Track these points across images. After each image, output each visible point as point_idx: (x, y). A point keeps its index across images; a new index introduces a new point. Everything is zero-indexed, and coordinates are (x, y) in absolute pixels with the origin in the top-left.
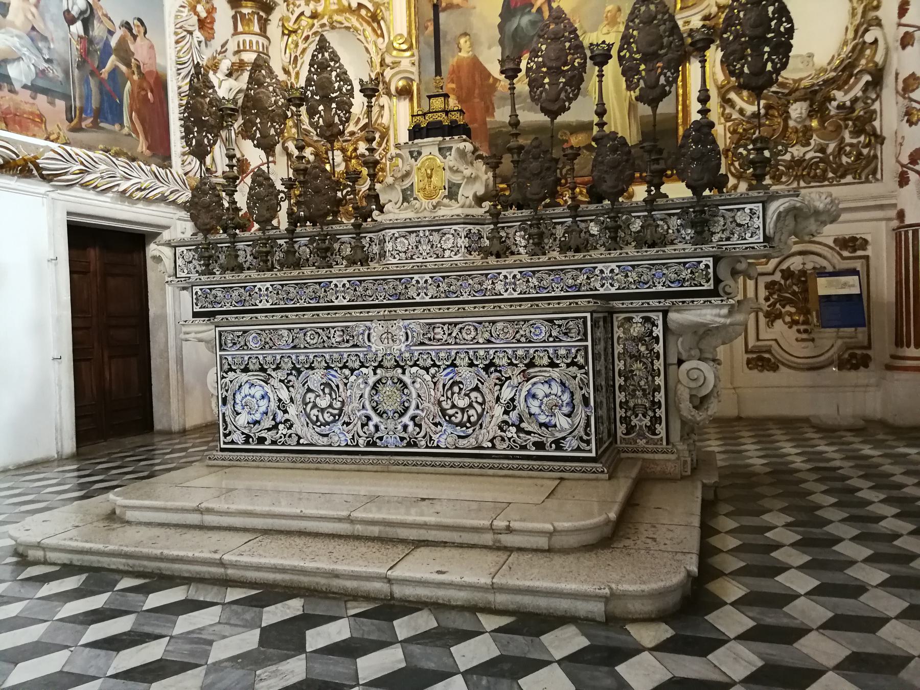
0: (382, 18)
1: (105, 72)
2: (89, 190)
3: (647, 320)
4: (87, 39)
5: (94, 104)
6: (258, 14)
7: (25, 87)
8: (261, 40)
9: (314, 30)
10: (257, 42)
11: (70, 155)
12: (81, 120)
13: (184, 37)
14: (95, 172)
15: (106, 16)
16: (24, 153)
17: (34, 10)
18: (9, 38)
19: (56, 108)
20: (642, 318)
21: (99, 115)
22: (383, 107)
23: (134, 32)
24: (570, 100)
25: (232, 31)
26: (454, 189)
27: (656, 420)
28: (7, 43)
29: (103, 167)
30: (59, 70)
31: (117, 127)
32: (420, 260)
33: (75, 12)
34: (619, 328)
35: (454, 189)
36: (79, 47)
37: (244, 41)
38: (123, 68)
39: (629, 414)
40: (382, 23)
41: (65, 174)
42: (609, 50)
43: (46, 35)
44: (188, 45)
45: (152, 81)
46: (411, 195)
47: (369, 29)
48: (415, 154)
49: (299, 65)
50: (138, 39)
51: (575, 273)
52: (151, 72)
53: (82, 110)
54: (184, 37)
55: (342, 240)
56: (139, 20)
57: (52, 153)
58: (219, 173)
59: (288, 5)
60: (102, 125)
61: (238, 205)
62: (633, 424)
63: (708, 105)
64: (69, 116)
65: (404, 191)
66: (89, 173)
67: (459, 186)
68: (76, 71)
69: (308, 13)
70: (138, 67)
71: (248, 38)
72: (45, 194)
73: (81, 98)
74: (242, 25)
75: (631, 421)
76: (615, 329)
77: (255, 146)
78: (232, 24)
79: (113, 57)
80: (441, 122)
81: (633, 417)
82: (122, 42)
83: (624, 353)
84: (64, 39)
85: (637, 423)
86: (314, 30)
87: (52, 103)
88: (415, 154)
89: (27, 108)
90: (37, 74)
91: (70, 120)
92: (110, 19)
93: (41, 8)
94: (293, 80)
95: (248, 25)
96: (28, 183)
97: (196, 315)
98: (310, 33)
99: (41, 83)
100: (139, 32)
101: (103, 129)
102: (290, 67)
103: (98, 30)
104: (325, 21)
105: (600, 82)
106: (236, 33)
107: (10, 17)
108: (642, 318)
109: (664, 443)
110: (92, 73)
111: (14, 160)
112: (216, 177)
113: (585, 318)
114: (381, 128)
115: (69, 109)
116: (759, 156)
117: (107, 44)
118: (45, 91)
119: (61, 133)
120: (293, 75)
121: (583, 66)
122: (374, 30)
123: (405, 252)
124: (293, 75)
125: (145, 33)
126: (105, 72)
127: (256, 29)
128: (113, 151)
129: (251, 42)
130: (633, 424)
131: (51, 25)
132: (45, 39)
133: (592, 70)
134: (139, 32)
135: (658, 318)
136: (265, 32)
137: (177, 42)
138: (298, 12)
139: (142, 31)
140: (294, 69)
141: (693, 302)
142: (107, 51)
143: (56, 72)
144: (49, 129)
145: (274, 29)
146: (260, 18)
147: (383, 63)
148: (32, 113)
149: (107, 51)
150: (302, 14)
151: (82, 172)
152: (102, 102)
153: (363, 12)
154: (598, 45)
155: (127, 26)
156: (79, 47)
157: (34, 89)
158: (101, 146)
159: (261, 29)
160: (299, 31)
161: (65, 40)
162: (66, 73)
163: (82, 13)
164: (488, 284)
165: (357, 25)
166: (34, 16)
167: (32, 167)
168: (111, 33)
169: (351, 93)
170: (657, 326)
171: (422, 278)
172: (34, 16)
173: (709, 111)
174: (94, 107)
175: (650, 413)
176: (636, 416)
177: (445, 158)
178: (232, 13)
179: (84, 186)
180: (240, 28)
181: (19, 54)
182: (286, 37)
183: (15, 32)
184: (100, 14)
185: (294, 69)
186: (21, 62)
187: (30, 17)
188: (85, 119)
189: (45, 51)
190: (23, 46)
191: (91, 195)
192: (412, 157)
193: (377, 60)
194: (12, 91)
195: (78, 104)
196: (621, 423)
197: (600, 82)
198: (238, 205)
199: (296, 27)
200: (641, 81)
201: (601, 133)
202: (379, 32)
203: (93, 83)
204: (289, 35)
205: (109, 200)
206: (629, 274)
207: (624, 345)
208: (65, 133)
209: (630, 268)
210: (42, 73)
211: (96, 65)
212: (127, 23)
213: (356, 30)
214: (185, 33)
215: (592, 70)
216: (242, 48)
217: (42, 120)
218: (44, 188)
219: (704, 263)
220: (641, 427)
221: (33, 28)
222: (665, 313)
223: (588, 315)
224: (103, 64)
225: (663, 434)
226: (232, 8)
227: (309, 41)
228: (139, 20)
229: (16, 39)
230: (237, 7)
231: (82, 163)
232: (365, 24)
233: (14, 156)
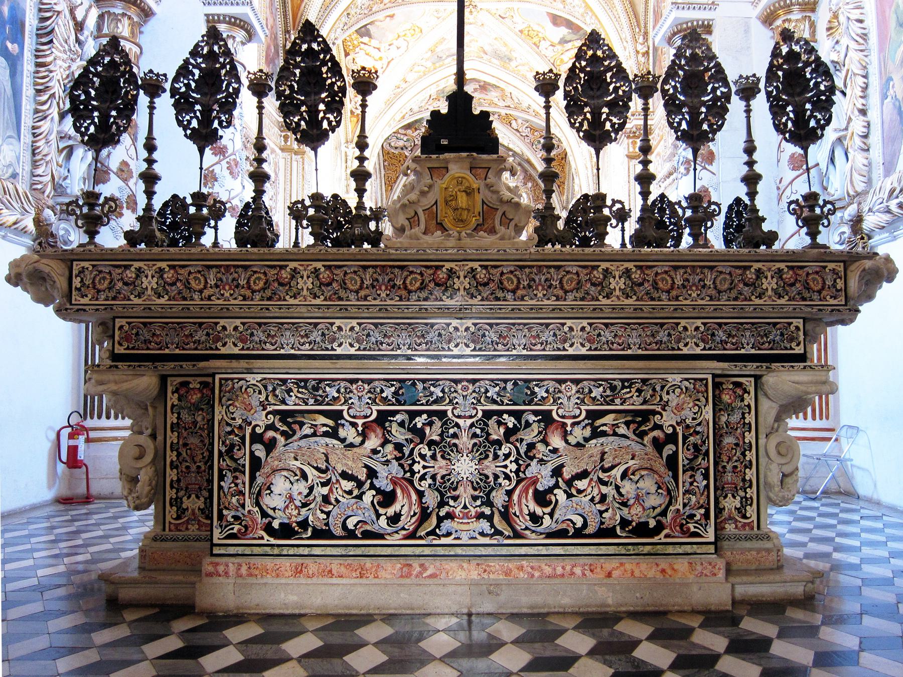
3: (738, 385)
20: (201, 383)
24: (714, 132)
27: (746, 502)
32: (533, 302)
34: (173, 393)
39: (181, 494)
42: (758, 83)
51: (656, 328)
55: (720, 269)
61: (760, 214)
62: (184, 506)
63: (649, 157)
75: (182, 503)
76: (169, 394)
77: (186, 135)
81: (185, 499)
83: (178, 423)
85: (189, 505)
97: (115, 357)
105: (151, 115)
108: (201, 383)
109: (755, 529)
113: (707, 379)
116: (812, 214)
121: (727, 97)
123: (668, 292)
130: (184, 506)
133: (736, 105)
135: (749, 383)
141: (139, 366)
154: (544, 74)
164: (662, 335)
169: (343, 90)
170: (749, 393)
171: (462, 325)
173: (651, 162)
175: (742, 494)
176: (189, 497)
196: (171, 505)
197: (151, 115)
198: (760, 214)
200: (684, 123)
201: (751, 173)
206: (487, 333)
207: (179, 414)
209: (716, 326)
215: (143, 99)
219: (221, 324)
220: (193, 510)
222: (757, 378)
223: (710, 377)
225: (754, 518)
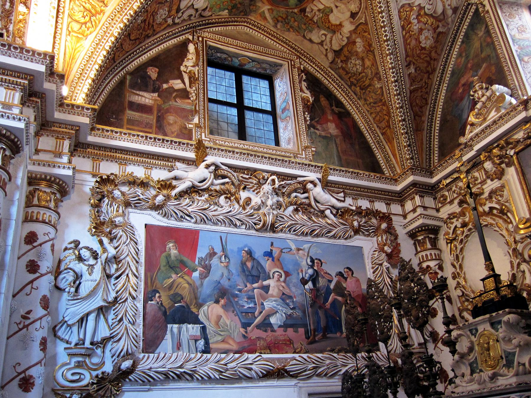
0: (508, 211)
1: (328, 305)
2: (323, 377)
4: (316, 290)
5: (323, 324)
6: (428, 237)
7: (280, 326)
8: (437, 252)
9: (465, 235)
10: (435, 254)
11: (305, 360)
12: (315, 336)
13: (378, 268)
14: (324, 366)
15: (326, 273)
16: (278, 365)
17: (283, 284)
18: (271, 303)
19: (299, 333)
21: (326, 330)
22: (524, 271)
23: (345, 276)
25: (415, 252)
26: (510, 357)
28: (269, 306)
29: (328, 362)
30: (300, 312)
31: (338, 334)
33: (307, 277)
35: (510, 357)
36: (310, 296)
37: (422, 256)
38: (340, 298)
40: (509, 214)
41: (305, 371)
43: (291, 295)
44: (380, 272)
45: (360, 301)
46: (477, 367)
47: (501, 221)
48: (474, 331)
49: (460, 260)
50: (348, 279)
52: (358, 296)
53: (315, 331)
54: (378, 268)
56: (348, 268)
57: (294, 361)
58: (416, 345)
59: (447, 225)
60: (328, 336)
64: (307, 336)
65: (471, 365)
66: (320, 368)
67: (514, 354)
68: (310, 309)
69: (459, 225)
70: (350, 295)
71: (424, 254)
72: (295, 385)
73: (313, 323)
74: (420, 247)
78: (414, 248)
79: (333, 294)
80: (493, 299)
82: (338, 284)
84: (301, 294)
86: (465, 235)
87: (296, 331)
88: (474, 331)
89: (282, 338)
90: (287, 318)
91: (308, 338)
92: (329, 274)
93: (287, 282)
94: (458, 270)
95: (423, 246)
96: (284, 381)
98: (463, 237)
99: (290, 322)
100: (348, 275)
101: (329, 338)
102: (455, 263)
103: (322, 282)
104: (470, 226)
106: (417, 253)
107: (270, 292)
110: (320, 307)
111: (272, 370)
112: (414, 349)
114: (526, 288)
115: (307, 332)
117: (328, 287)
118: (291, 326)
119: (303, 347)
120: (458, 267)
122: (505, 221)
124: (458, 267)
125: (353, 274)
126: (328, 305)
127: (429, 246)
128: (337, 350)
129: (426, 255)
131: (293, 289)
132: (290, 297)
134: (348, 275)
136: (435, 246)
137: (374, 273)
138: (453, 227)
139: (350, 273)
140: (457, 263)
142: (328, 292)
143: (298, 313)
144: (296, 346)
145: (442, 242)
146: (430, 239)
147: (516, 242)
148: (284, 340)
149: (328, 292)
150: (456, 227)
151: (314, 368)
152: (327, 323)
153: (495, 212)
155: (340, 274)
156: (310, 296)
157: (285, 326)
158: (329, 348)
159: (432, 245)
160: (457, 238)
161: (301, 294)
162: (304, 312)
163: (311, 276)
165: (493, 222)
166: (284, 287)
167: (283, 372)
168: (330, 281)
172: (284, 287)
174: (322, 326)
177: (497, 331)
178: (413, 242)
179: (319, 375)
180: (419, 249)
181: (276, 310)
182: (449, 245)
183: (273, 299)
184: (322, 273)
185: (457, 263)
186: (277, 314)
187: (281, 288)
188: (318, 335)
189: (291, 304)
190: (278, 305)
191: (324, 380)
192: (472, 334)
193: (511, 240)
194: (273, 331)
195: (312, 327)
199: (454, 236)
202: (509, 220)
203: (321, 313)
204: (451, 243)
205: (337, 380)
208: (305, 345)
210: (289, 316)
211: (322, 302)
212: (340, 272)
213: (492, 225)
214: (377, 266)
216: (425, 259)
217: (291, 343)
218: (293, 382)
221: (283, 294)
224: (326, 300)
226: (412, 239)
227: (463, 242)
228: (348, 268)
229: (274, 302)
230: (415, 238)
231: (314, 363)
232: (497, 219)
233: (272, 368)
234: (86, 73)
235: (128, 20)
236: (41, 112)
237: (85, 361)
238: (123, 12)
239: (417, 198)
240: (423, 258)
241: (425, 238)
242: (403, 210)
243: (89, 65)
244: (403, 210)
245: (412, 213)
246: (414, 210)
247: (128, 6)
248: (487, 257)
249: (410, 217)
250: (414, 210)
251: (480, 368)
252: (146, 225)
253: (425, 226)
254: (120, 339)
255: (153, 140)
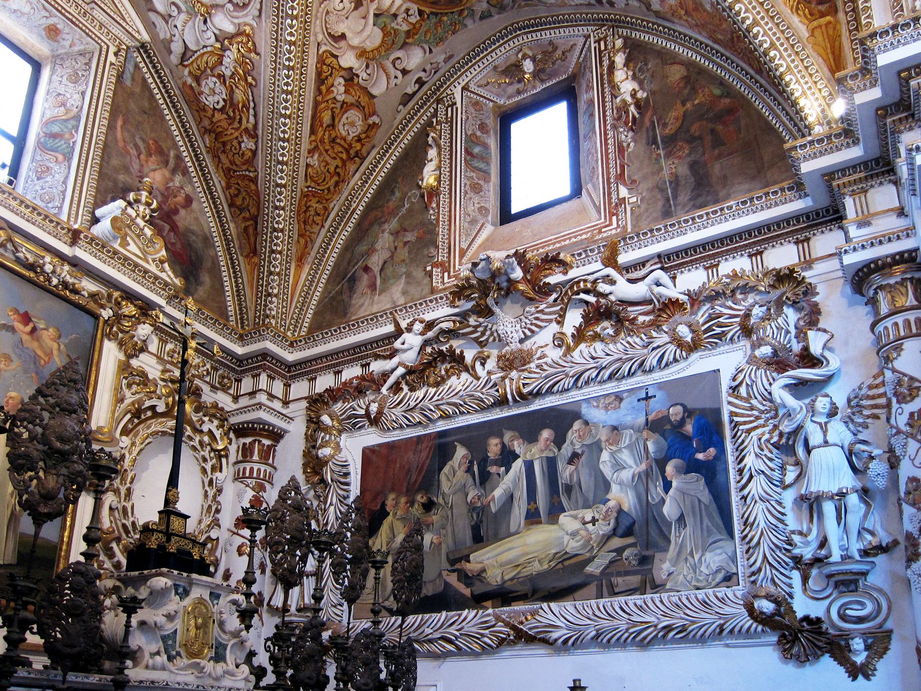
8: (269, 469)
10: (265, 471)
216: (247, 475)
234: (789, 56)
235: (738, 13)
236: (887, 143)
237: (541, 608)
238: (789, 56)
239: (264, 377)
240: (244, 473)
241: (255, 441)
242: (286, 393)
243: (770, 25)
244: (286, 393)
245: (247, 398)
246: (252, 394)
247: (782, 45)
248: (173, 481)
249: (244, 402)
250: (252, 394)
251: (178, 649)
252: (719, 370)
253: (259, 424)
254: (758, 543)
255: (691, 222)
